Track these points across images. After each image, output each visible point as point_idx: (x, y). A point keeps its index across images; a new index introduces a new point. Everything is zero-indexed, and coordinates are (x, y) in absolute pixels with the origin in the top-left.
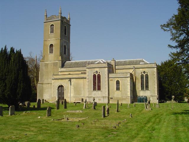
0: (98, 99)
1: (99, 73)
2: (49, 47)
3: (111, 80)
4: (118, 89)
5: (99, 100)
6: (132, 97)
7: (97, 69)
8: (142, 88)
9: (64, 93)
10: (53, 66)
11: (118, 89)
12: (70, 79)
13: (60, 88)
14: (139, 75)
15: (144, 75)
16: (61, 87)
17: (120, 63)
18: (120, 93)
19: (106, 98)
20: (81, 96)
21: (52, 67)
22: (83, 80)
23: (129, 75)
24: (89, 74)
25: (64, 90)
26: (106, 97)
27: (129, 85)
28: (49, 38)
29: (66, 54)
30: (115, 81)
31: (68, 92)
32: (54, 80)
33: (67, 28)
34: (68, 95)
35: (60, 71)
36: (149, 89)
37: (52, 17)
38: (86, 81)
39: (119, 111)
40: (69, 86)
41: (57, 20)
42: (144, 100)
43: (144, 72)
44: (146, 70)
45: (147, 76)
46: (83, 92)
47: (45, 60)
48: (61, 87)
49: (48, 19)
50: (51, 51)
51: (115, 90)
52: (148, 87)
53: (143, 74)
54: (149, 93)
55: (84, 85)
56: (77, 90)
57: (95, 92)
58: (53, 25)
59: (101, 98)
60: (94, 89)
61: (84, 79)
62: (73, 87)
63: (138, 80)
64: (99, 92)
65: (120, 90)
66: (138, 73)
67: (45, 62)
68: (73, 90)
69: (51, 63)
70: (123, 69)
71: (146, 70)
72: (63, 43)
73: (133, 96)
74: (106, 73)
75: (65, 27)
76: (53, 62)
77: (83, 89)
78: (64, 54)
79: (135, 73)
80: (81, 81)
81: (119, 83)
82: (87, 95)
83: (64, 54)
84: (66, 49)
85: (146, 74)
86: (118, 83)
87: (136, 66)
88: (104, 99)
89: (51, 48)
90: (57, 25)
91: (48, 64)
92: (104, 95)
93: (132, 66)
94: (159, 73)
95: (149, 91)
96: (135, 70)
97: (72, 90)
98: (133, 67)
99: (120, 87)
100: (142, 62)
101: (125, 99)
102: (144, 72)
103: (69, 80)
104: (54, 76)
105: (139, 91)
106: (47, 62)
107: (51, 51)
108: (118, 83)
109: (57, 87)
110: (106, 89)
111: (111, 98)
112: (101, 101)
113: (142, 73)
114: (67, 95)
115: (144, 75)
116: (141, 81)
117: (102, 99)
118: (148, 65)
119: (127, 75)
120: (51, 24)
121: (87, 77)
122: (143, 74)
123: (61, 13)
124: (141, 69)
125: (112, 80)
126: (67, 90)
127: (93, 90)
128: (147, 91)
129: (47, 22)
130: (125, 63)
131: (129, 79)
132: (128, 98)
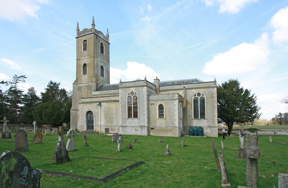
0: (134, 130)
1: (136, 94)
2: (82, 68)
3: (151, 104)
4: (161, 115)
5: (136, 130)
6: (181, 128)
7: (133, 90)
8: (196, 116)
9: (93, 121)
10: (86, 89)
11: (161, 115)
12: (100, 104)
13: (89, 116)
14: (192, 97)
15: (199, 98)
16: (89, 113)
17: (166, 84)
18: (164, 122)
19: (144, 128)
20: (113, 125)
21: (86, 91)
22: (116, 104)
23: (176, 96)
24: (123, 95)
25: (93, 117)
26: (144, 126)
27: (177, 111)
28: (82, 57)
29: (103, 76)
30: (157, 105)
31: (98, 120)
32: (82, 104)
33: (104, 46)
34: (98, 123)
35: (93, 94)
36: (206, 118)
37: (85, 30)
38: (119, 105)
39: (215, 80)
40: (98, 112)
41: (89, 34)
42: (199, 132)
43: (199, 94)
44: (201, 91)
45: (203, 101)
46: (115, 120)
47: (79, 82)
48: (89, 113)
49: (80, 34)
50: (85, 73)
51: (158, 117)
52: (205, 115)
53: (197, 96)
54: (206, 124)
55: (116, 111)
56: (109, 116)
57: (130, 120)
58: (85, 41)
59: (137, 128)
60: (130, 116)
61: (117, 103)
62: (103, 114)
63: (190, 105)
64: (136, 120)
65: (138, 117)
66: (191, 95)
67: (79, 85)
68: (103, 117)
69: (84, 86)
70: (170, 90)
71: (201, 91)
72: (98, 63)
73: (183, 126)
74: (144, 95)
75: (101, 43)
76: (87, 84)
77: (115, 116)
78: (101, 75)
79: (185, 95)
80: (113, 105)
81: (163, 108)
82: (120, 125)
83: (101, 75)
84: (104, 71)
85: (201, 96)
86: (161, 107)
87: (187, 86)
88: (141, 129)
89: (85, 68)
90: (90, 39)
91: (82, 87)
92: (143, 125)
93: (182, 87)
94: (219, 97)
95: (205, 121)
96: (186, 92)
97: (103, 117)
98: (183, 88)
99: (164, 113)
100: (194, 82)
101: (170, 131)
102: (199, 94)
103: (98, 104)
104: (82, 100)
105: (191, 120)
106: (81, 85)
107: (85, 73)
108: (161, 107)
109: (85, 113)
110: (144, 116)
111: (153, 129)
112: (138, 132)
113: (195, 95)
114: (96, 123)
115: (199, 98)
116: (194, 106)
117: (139, 129)
118: (204, 85)
119: (173, 97)
120: (83, 40)
121: (120, 101)
122: (197, 96)
123: (94, 25)
124: (194, 90)
125: (153, 104)
126: (96, 117)
127: (127, 118)
128: (202, 120)
129: (79, 37)
130: (173, 84)
131: (176, 102)
132: (175, 129)
